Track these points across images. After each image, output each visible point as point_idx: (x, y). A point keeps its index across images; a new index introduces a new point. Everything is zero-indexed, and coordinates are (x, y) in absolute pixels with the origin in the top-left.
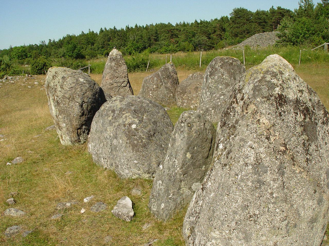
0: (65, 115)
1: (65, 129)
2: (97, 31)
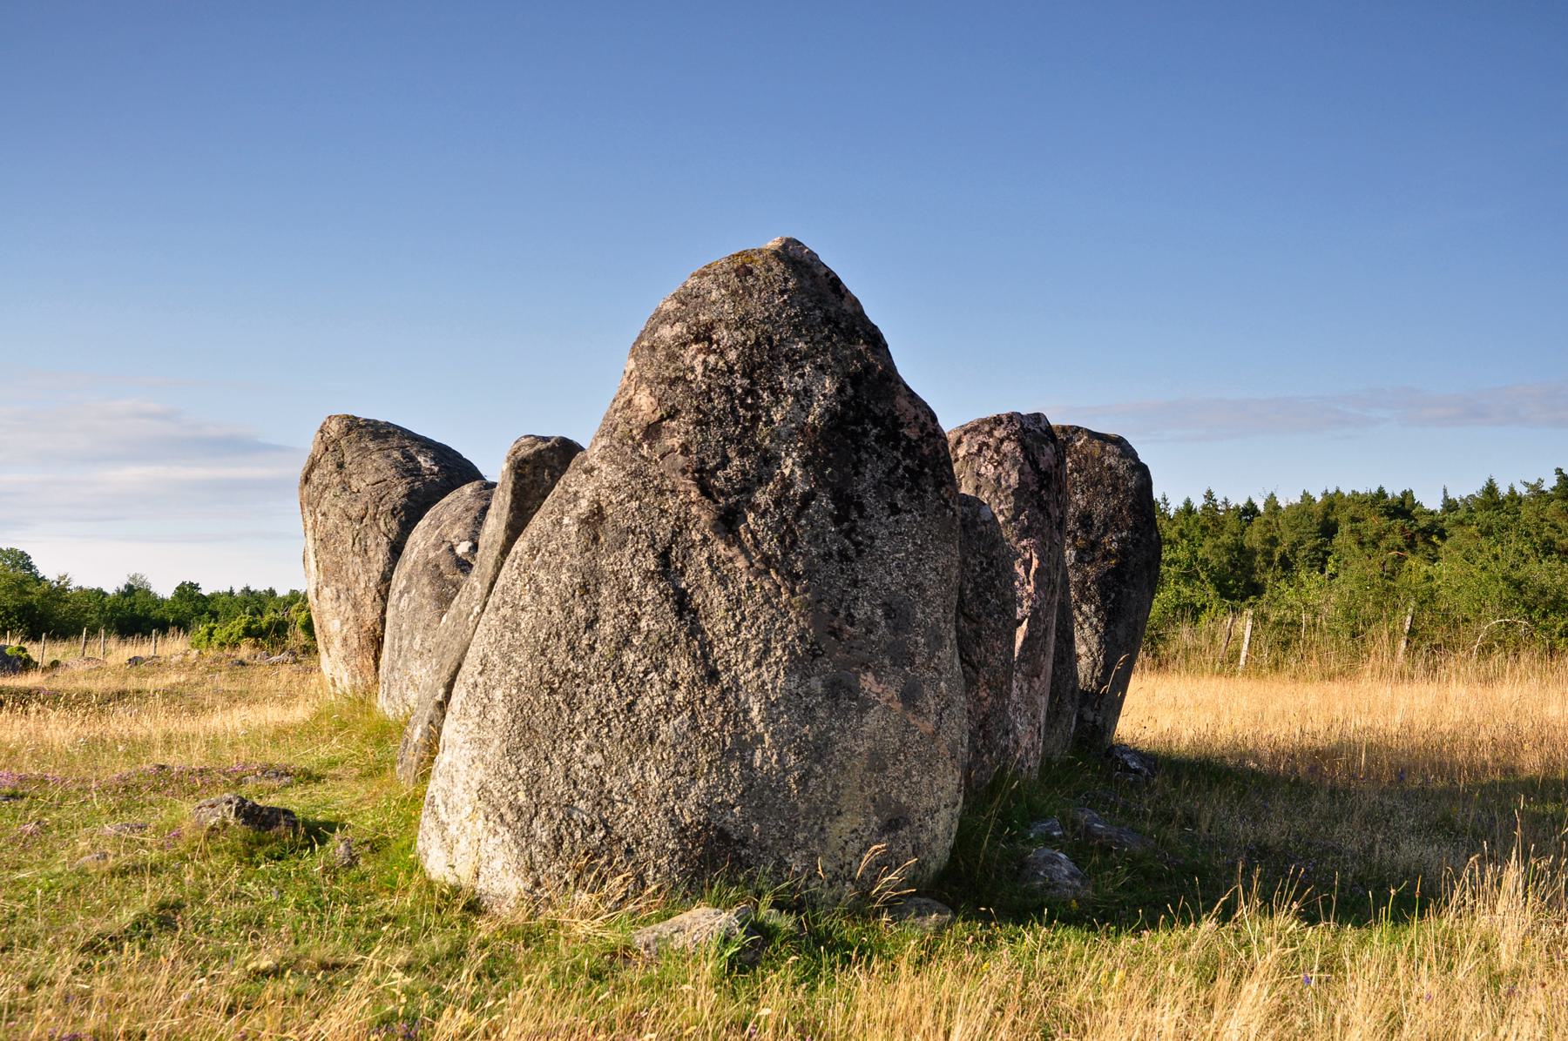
0: (340, 586)
1: (337, 643)
2: (1347, 492)
